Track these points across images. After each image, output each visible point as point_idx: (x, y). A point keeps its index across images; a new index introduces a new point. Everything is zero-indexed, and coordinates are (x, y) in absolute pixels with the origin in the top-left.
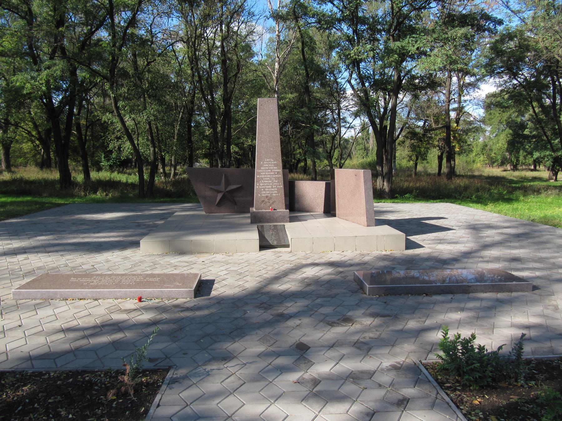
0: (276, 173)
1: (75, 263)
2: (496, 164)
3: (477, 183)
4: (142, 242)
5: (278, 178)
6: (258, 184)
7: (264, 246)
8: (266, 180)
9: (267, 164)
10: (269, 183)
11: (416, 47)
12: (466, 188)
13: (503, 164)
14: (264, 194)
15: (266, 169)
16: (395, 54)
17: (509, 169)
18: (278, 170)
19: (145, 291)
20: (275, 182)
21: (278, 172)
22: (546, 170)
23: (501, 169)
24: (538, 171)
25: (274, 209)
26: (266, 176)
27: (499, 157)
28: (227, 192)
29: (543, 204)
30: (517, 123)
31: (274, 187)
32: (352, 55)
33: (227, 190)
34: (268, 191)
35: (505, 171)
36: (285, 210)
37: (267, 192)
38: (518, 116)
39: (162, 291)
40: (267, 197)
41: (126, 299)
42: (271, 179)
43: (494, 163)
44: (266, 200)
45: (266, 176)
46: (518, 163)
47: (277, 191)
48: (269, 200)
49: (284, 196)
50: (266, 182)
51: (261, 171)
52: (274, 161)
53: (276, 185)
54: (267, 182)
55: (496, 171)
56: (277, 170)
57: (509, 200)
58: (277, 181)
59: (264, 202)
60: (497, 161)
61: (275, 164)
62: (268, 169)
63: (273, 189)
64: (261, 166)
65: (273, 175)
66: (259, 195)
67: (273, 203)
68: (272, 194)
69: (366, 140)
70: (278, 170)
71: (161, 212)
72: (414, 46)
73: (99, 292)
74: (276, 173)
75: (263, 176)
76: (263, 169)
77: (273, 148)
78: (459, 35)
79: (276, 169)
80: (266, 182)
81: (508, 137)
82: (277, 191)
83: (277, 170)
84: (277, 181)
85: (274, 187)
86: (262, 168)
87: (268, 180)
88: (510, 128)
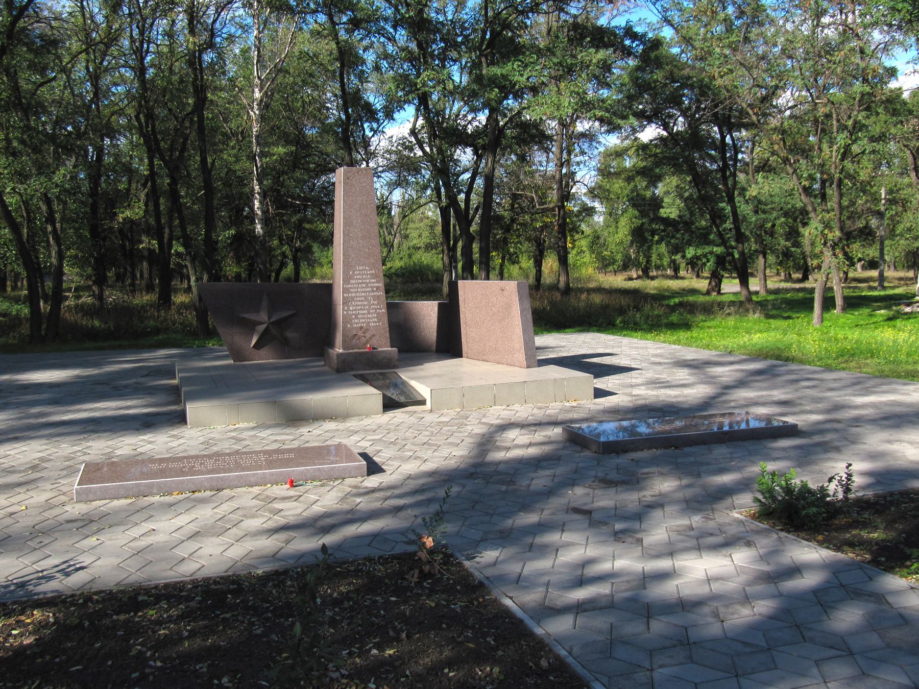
0: (375, 289)
1: (57, 455)
2: (611, 268)
3: (624, 301)
4: (193, 409)
5: (379, 297)
6: (346, 308)
7: (389, 405)
8: (359, 301)
9: (359, 274)
10: (364, 305)
11: (525, 77)
12: (604, 308)
13: (625, 267)
14: (356, 323)
15: (358, 283)
16: (495, 87)
17: (635, 276)
18: (378, 285)
19: (293, 471)
20: (373, 304)
21: (378, 288)
22: (694, 277)
23: (625, 275)
24: (683, 278)
25: (374, 348)
26: (358, 294)
27: (619, 257)
28: (272, 323)
29: (726, 330)
30: (644, 199)
31: (371, 311)
32: (418, 87)
33: (271, 320)
34: (363, 318)
35: (631, 279)
36: (390, 349)
37: (361, 321)
38: (647, 187)
39: (319, 469)
40: (361, 328)
41: (265, 485)
42: (366, 298)
43: (606, 266)
44: (360, 333)
45: (358, 294)
46: (648, 266)
47: (377, 317)
48: (364, 333)
49: (387, 325)
50: (359, 303)
51: (350, 286)
52: (371, 270)
53: (376, 309)
54: (361, 303)
55: (618, 281)
56: (375, 285)
57: (687, 326)
58: (376, 302)
59: (357, 337)
60: (614, 262)
61: (371, 274)
62: (362, 283)
63: (371, 316)
64: (351, 278)
65: (369, 292)
66: (349, 326)
67: (371, 338)
68: (369, 323)
69: (387, 228)
70: (378, 285)
71: (137, 365)
72: (522, 75)
73: (222, 479)
74: (375, 289)
75: (354, 295)
76: (353, 284)
77: (369, 249)
78: (594, 61)
79: (374, 283)
80: (359, 303)
81: (633, 223)
82: (377, 317)
83: (375, 285)
84: (376, 302)
85: (371, 311)
86: (352, 281)
87: (362, 301)
88: (634, 206)
